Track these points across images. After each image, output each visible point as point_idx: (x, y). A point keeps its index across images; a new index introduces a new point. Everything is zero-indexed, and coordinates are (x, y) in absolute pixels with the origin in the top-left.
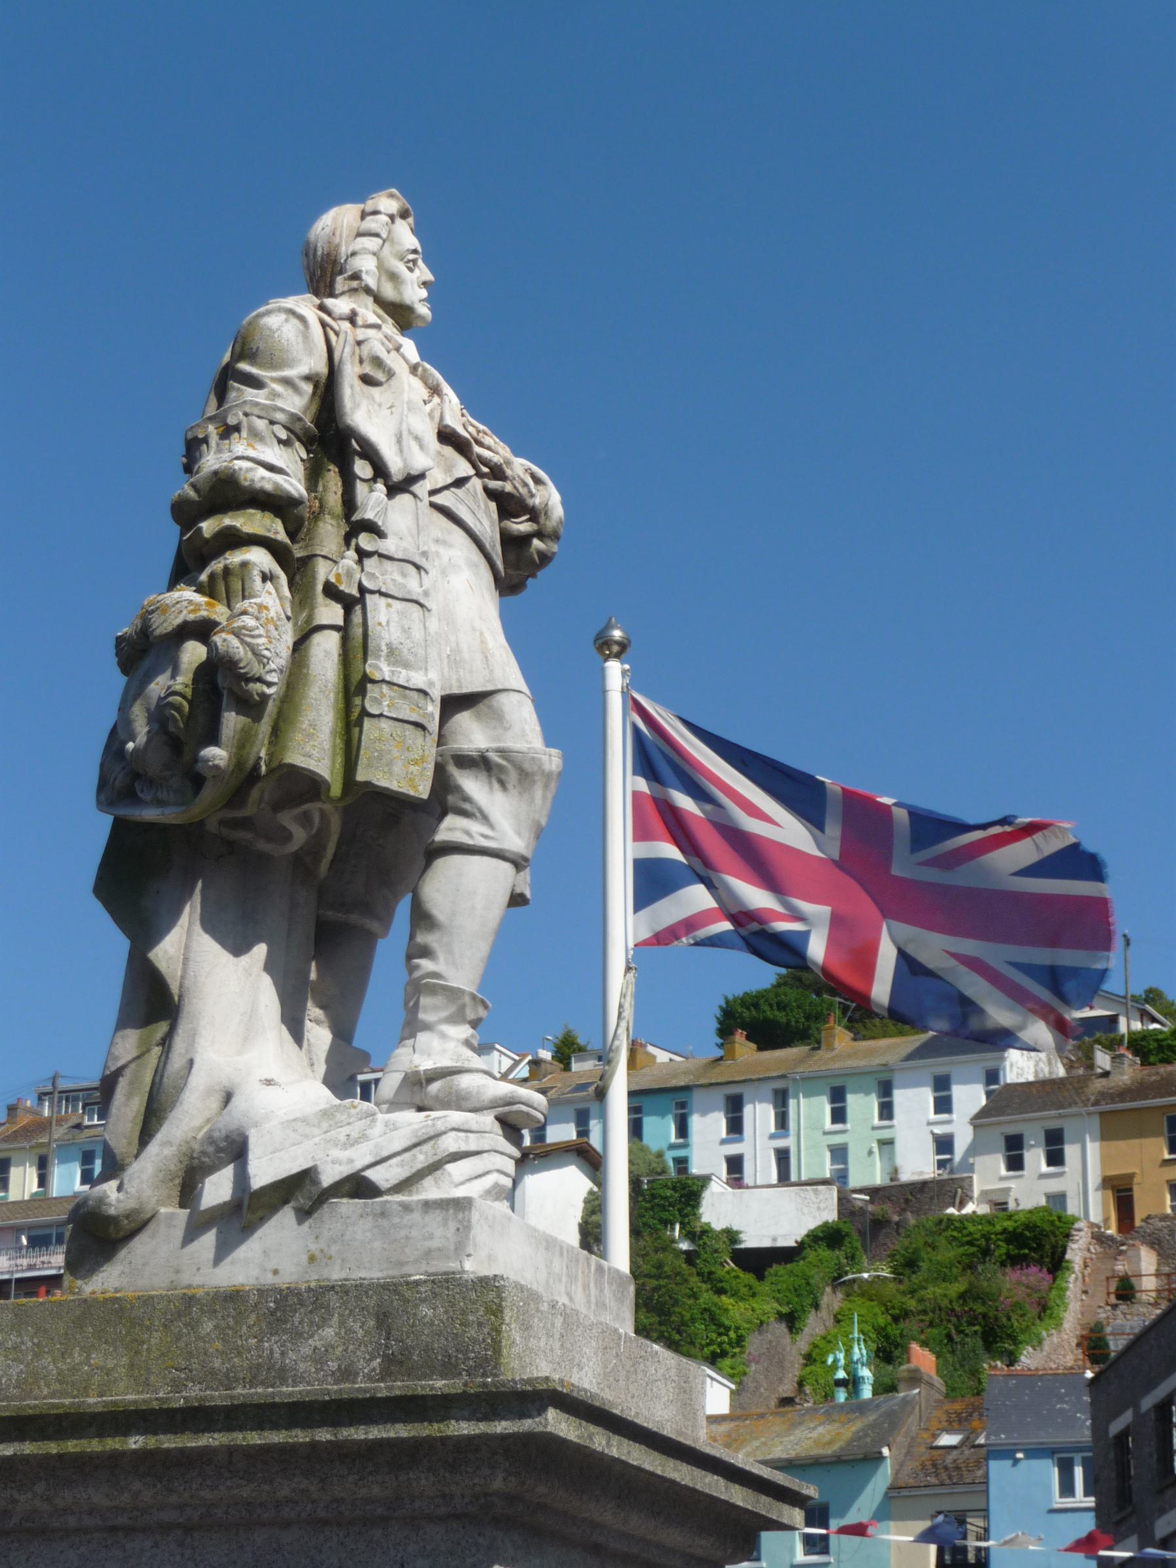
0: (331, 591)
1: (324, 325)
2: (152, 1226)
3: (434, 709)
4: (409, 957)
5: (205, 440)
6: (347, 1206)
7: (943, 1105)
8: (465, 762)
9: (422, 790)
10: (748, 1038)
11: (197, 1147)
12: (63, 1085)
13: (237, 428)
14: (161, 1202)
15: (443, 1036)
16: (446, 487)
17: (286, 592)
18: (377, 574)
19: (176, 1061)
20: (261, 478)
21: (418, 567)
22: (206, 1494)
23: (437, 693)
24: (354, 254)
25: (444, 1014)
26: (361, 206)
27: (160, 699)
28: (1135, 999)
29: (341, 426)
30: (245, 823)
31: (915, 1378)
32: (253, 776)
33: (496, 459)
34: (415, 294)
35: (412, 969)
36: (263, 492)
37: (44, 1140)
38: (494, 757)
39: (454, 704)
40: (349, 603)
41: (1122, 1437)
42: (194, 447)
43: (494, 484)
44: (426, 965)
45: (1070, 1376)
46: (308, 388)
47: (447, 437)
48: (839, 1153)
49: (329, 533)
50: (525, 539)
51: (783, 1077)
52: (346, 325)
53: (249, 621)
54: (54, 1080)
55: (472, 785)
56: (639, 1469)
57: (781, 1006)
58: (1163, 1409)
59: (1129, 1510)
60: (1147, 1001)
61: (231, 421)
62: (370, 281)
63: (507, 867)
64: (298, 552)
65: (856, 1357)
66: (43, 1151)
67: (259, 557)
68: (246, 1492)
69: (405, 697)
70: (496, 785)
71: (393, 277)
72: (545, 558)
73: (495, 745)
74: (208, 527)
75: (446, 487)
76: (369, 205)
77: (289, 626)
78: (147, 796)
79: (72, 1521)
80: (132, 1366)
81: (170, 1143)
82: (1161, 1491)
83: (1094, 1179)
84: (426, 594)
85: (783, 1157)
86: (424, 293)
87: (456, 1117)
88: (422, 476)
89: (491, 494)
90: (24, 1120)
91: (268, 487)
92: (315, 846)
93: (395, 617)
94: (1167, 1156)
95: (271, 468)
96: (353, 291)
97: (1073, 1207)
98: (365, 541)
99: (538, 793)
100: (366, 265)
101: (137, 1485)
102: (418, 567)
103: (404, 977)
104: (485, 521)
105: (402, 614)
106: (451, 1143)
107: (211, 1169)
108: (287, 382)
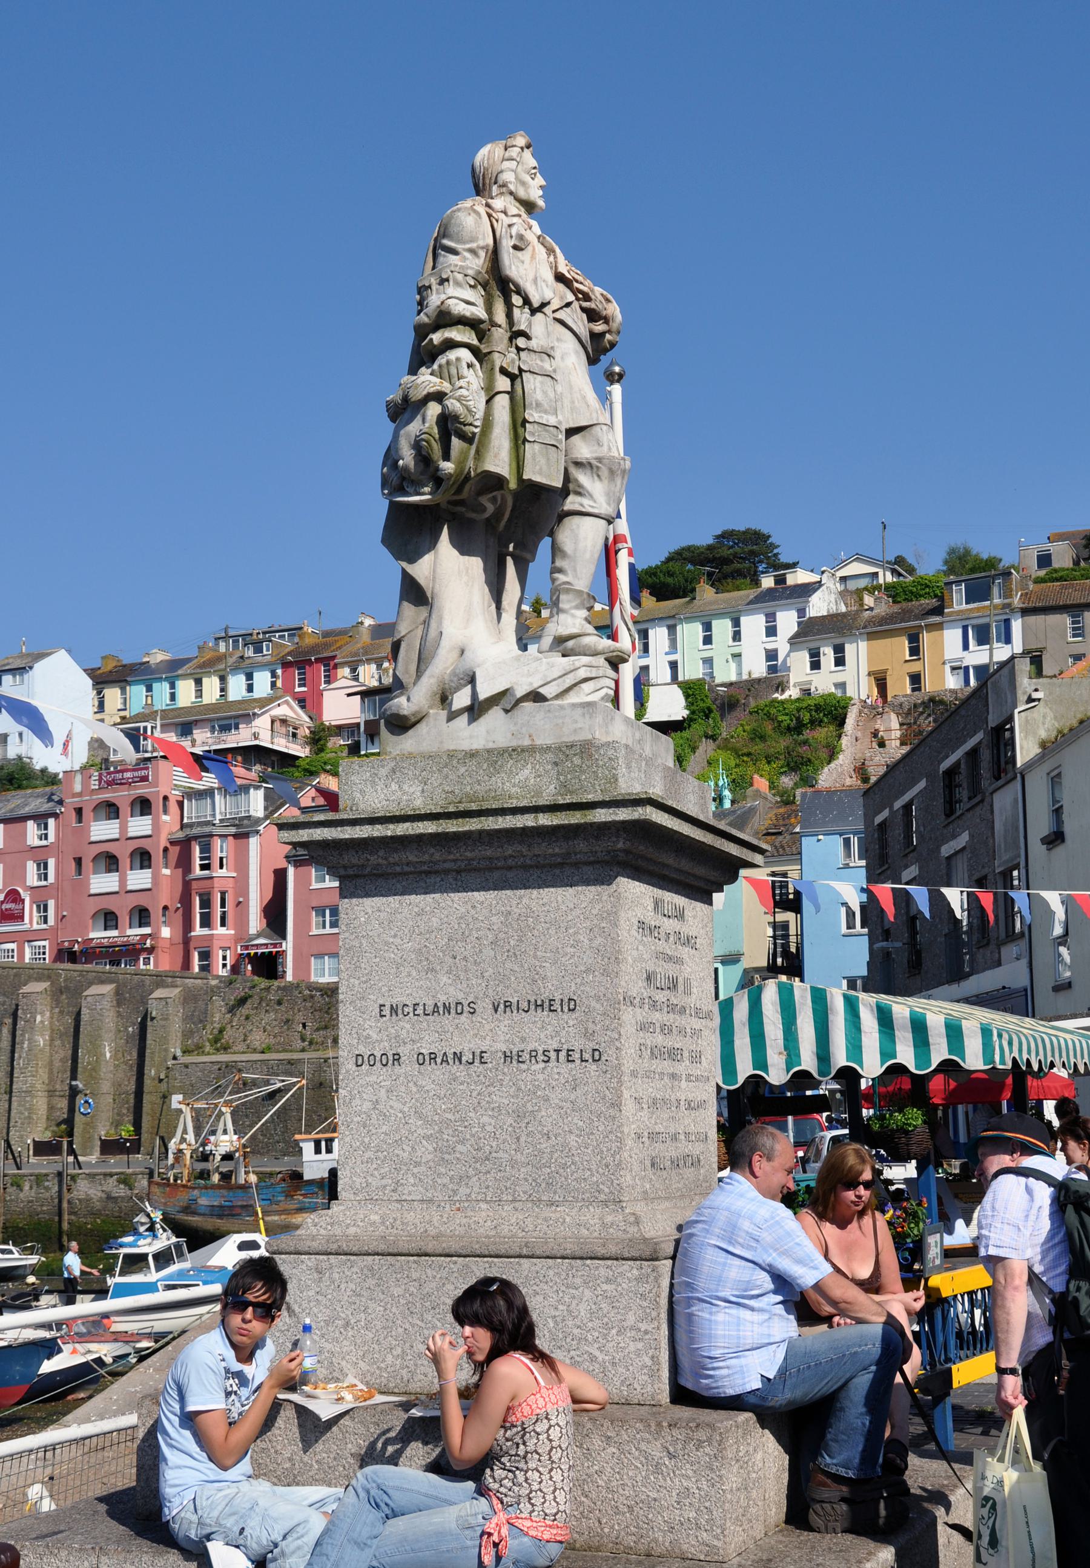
0: (504, 371)
1: (489, 216)
2: (425, 720)
3: (562, 436)
4: (552, 573)
5: (430, 287)
6: (528, 705)
7: (771, 631)
8: (578, 464)
9: (558, 483)
10: (651, 594)
11: (446, 677)
12: (231, 633)
13: (447, 280)
14: (431, 707)
15: (573, 616)
16: (561, 308)
17: (480, 373)
18: (528, 361)
19: (433, 633)
20: (459, 308)
21: (549, 356)
22: (468, 854)
23: (563, 428)
24: (502, 172)
25: (574, 604)
26: (504, 142)
27: (417, 436)
28: (888, 562)
29: (503, 274)
30: (461, 503)
31: (758, 794)
32: (468, 478)
33: (585, 289)
34: (535, 194)
35: (553, 580)
36: (464, 317)
37: (222, 666)
38: (594, 462)
39: (571, 432)
40: (513, 377)
41: (883, 825)
42: (423, 290)
43: (585, 304)
44: (561, 578)
45: (848, 792)
46: (482, 254)
47: (560, 278)
48: (708, 662)
49: (500, 335)
50: (602, 335)
51: (673, 617)
52: (502, 216)
53: (463, 392)
54: (226, 630)
55: (583, 478)
56: (688, 837)
57: (670, 574)
58: (907, 807)
59: (886, 866)
60: (895, 563)
61: (444, 276)
62: (512, 187)
63: (604, 522)
64: (484, 349)
65: (721, 783)
66: (221, 673)
67: (465, 354)
68: (489, 853)
69: (547, 431)
70: (596, 478)
71: (523, 183)
72: (613, 345)
73: (595, 455)
74: (437, 338)
75: (561, 308)
76: (510, 142)
77: (483, 393)
78: (410, 490)
79: (398, 869)
80: (423, 791)
81: (433, 676)
82: (906, 855)
83: (864, 670)
84: (555, 371)
85: (674, 665)
86: (541, 193)
87: (585, 660)
88: (549, 303)
89: (583, 309)
90: (208, 655)
91: (468, 314)
92: (498, 514)
93: (538, 385)
94: (908, 658)
95: (468, 303)
96: (502, 194)
97: (851, 692)
98: (521, 342)
99: (619, 481)
100: (508, 177)
101: (432, 850)
102: (549, 356)
103: (550, 585)
104: (581, 324)
105: (542, 383)
106: (583, 673)
107: (457, 689)
108: (472, 251)
